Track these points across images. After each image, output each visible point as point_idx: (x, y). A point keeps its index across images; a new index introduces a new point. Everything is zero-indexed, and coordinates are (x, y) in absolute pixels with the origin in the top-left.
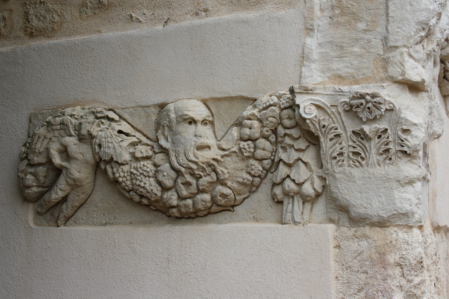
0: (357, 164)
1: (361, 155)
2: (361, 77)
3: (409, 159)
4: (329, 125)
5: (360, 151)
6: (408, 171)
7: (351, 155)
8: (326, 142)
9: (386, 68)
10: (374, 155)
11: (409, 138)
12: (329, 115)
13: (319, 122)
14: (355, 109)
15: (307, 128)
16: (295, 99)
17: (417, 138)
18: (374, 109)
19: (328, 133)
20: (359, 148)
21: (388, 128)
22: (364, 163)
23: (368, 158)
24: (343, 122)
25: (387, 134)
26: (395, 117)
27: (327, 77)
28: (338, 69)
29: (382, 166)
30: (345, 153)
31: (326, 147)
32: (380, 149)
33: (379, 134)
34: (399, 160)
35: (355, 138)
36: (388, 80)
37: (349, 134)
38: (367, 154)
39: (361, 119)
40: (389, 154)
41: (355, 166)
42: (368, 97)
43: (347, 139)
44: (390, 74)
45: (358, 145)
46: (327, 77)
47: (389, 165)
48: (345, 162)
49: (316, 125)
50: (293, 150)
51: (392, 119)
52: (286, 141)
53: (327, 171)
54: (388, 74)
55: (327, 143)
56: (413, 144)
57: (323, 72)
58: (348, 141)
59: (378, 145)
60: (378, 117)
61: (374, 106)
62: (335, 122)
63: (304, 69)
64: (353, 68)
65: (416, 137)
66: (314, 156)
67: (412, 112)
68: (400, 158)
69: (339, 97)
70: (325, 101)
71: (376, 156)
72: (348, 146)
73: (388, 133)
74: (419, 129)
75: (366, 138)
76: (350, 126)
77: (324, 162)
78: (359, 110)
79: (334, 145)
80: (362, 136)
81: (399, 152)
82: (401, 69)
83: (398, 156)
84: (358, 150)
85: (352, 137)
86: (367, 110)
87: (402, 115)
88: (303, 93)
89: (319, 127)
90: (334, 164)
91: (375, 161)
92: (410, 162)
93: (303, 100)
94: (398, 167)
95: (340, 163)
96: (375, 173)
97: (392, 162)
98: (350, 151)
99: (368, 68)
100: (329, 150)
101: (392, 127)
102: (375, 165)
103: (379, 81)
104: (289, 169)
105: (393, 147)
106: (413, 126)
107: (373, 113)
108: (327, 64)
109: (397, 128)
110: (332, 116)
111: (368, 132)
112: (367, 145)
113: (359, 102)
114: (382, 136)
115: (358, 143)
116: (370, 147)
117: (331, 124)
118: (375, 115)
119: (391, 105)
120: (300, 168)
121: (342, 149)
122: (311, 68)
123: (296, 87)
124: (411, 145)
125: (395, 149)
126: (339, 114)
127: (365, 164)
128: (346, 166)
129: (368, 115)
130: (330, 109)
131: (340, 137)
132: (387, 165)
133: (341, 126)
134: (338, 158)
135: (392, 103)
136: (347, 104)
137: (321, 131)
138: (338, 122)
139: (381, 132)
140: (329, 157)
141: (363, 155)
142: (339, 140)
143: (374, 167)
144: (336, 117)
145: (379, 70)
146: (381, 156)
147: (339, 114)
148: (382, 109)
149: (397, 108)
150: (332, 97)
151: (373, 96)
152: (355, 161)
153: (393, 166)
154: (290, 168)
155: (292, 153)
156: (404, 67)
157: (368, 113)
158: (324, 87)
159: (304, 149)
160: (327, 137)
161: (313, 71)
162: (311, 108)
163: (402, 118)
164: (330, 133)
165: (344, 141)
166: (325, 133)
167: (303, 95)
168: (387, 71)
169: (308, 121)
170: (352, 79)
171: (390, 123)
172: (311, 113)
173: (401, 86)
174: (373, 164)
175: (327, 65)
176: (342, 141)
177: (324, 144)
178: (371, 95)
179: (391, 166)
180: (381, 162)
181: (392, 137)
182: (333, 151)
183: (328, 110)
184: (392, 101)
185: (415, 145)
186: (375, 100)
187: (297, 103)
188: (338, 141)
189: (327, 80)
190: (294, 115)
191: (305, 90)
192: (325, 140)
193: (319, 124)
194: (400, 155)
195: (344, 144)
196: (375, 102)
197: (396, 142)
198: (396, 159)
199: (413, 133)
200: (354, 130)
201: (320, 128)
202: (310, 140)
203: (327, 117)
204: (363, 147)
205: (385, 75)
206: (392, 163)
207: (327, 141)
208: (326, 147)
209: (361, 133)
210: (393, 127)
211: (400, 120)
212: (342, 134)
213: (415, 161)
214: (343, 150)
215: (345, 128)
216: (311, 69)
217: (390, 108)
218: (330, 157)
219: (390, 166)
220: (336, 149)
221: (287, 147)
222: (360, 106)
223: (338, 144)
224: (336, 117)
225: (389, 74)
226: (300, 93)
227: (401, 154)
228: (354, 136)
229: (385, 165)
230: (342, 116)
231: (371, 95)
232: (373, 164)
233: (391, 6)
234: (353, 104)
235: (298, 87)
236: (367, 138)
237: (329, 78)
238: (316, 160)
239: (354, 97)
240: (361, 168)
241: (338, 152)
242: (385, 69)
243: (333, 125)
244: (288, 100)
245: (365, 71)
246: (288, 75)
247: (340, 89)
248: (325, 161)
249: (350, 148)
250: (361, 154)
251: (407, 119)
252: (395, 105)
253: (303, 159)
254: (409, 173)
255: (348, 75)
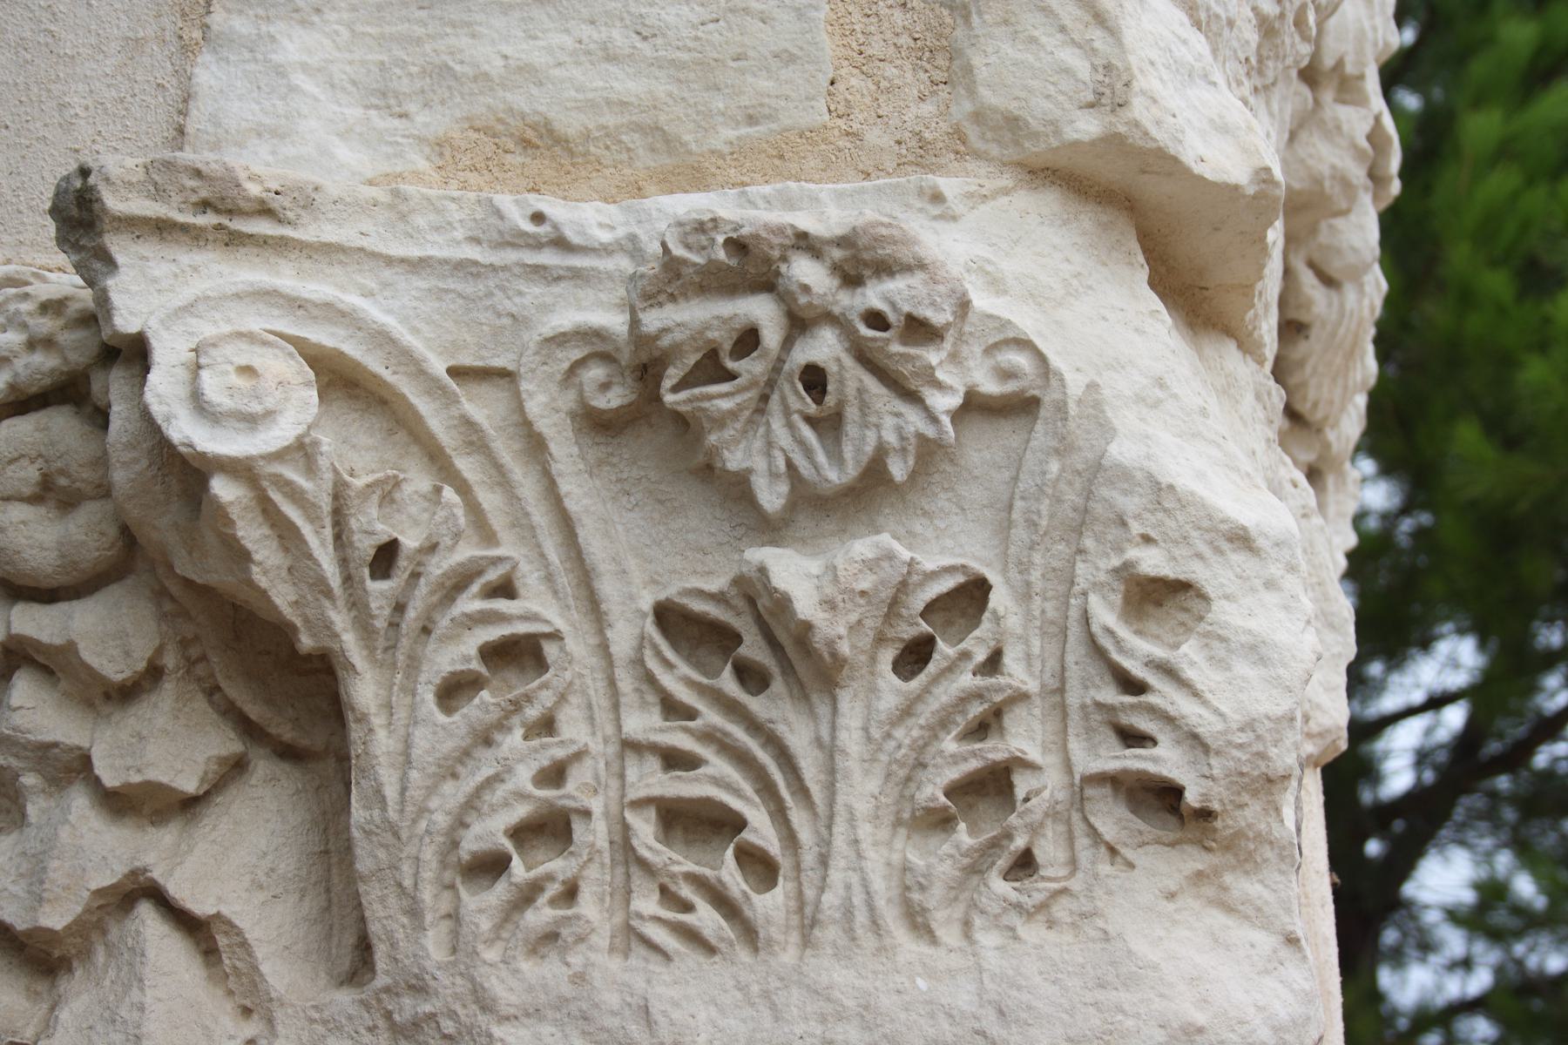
0: (706, 917)
1: (746, 835)
2: (729, 133)
3: (1194, 860)
4: (432, 548)
5: (737, 792)
6: (1193, 981)
7: (645, 829)
8: (401, 714)
9: (953, 54)
10: (865, 831)
11: (1190, 655)
12: (436, 458)
13: (339, 516)
14: (683, 395)
15: (215, 574)
16: (110, 283)
17: (1263, 661)
18: (861, 391)
19: (426, 631)
20: (719, 765)
21: (993, 577)
22: (769, 905)
23: (809, 858)
24: (566, 524)
25: (985, 628)
26: (1054, 467)
27: (421, 140)
28: (527, 71)
29: (949, 935)
30: (586, 814)
31: (406, 759)
32: (922, 775)
33: (908, 632)
34: (1105, 868)
35: (678, 678)
36: (978, 155)
37: (622, 639)
38: (798, 817)
39: (738, 490)
40: (1013, 819)
41: (692, 936)
42: (806, 272)
43: (612, 683)
44: (987, 96)
45: (710, 736)
46: (421, 140)
47: (1013, 919)
48: (588, 906)
49: (307, 530)
50: (79, 802)
51: (1026, 483)
52: (18, 719)
53: (407, 1001)
54: (972, 92)
55: (414, 721)
56: (1236, 718)
57: (384, 98)
58: (616, 707)
59: (899, 733)
60: (898, 470)
61: (865, 357)
62: (497, 521)
63: (208, 74)
64: (658, 63)
65: (1257, 651)
66: (287, 865)
67: (1196, 435)
68: (1113, 851)
69: (535, 291)
70: (404, 320)
71: (889, 844)
72: (612, 749)
73: (997, 619)
74: (1270, 585)
75: (788, 669)
76: (632, 563)
77: (383, 914)
78: (720, 398)
79: (485, 739)
80: (753, 648)
81: (1107, 790)
82: (1087, 49)
83: (1094, 833)
84: (717, 781)
85: (652, 664)
86: (794, 404)
87: (1122, 451)
88: (184, 228)
89: (344, 562)
90: (485, 924)
91: (878, 884)
92: (1209, 891)
93: (187, 294)
94: (1106, 937)
95: (540, 915)
96: (886, 1001)
97: (1037, 890)
98: (633, 794)
99: (792, 59)
100: (431, 790)
101: (1024, 567)
102: (875, 925)
103: (890, 165)
104: (34, 996)
105: (1045, 750)
106: (1218, 551)
107: (851, 429)
108: (419, 31)
109: (1081, 568)
110: (467, 466)
111: (806, 605)
112: (799, 738)
113: (724, 321)
114: (941, 644)
115: (711, 717)
116: (829, 751)
117: (457, 536)
118: (869, 449)
119: (1021, 360)
120: (147, 972)
121: (555, 775)
122: (277, 58)
123: (114, 171)
124: (1220, 727)
125: (1068, 766)
126: (535, 446)
127: (779, 916)
128: (601, 940)
129: (808, 453)
130: (450, 399)
131: (541, 665)
132: (996, 922)
133: (554, 556)
134: (519, 870)
135: (1024, 344)
136: (606, 358)
137: (358, 606)
138: (522, 524)
139: (929, 610)
140: (429, 854)
141: (761, 830)
142: (528, 698)
143: (868, 941)
144: (502, 479)
145: (890, 71)
146: (934, 840)
147: (535, 446)
148: (939, 385)
149: (1075, 385)
150: (468, 288)
151: (857, 260)
152: (686, 891)
153: (1051, 936)
154: (41, 986)
155: (64, 834)
156: (1113, 32)
157: (807, 432)
158: (396, 193)
159: (189, 784)
160: (414, 664)
161: (293, 89)
162: (256, 363)
163: (1123, 475)
164: (443, 623)
165: (574, 700)
166: (394, 625)
167: (188, 257)
168: (969, 70)
169: (223, 489)
170: (645, 159)
171: (1010, 524)
172: (256, 408)
173: (1088, 218)
174: (861, 918)
175: (419, 41)
176: (562, 698)
177: (381, 734)
178: (837, 254)
179: (1032, 933)
180: (938, 891)
181: (1028, 657)
182: (472, 804)
183: (424, 406)
184: (1026, 321)
185: (1249, 725)
186: (874, 295)
187: (126, 321)
188: (517, 706)
189: (422, 165)
190: (102, 461)
191: (205, 205)
192: (401, 701)
193: (338, 537)
194: (1111, 818)
195: (573, 729)
196: (876, 320)
197: (1073, 699)
198: (1073, 863)
199: (1227, 614)
200: (670, 592)
201: (348, 579)
202: (254, 711)
203: (418, 481)
204: (764, 757)
205: (944, 112)
206: (1043, 907)
207: (413, 708)
208: (406, 759)
209: (743, 624)
210: (1037, 558)
211: (1105, 492)
212: (555, 636)
213: (1244, 886)
214: (574, 790)
215: (585, 576)
216: (280, 71)
217: (1010, 387)
218: (444, 865)
219: (1022, 931)
220: (496, 779)
221: (29, 780)
222: (730, 365)
223: (518, 733)
224: (502, 479)
225: (985, 93)
226: (162, 228)
227: (1122, 811)
228: (669, 654)
229: (978, 921)
230: (555, 468)
231: (837, 254)
232: (861, 918)
233: (609, 402)
234: (665, 342)
235: (140, 175)
236: (802, 669)
237: (440, 146)
238: (311, 905)
239: (672, 266)
240: (743, 955)
241: (521, 812)
242: (941, 61)
243: (466, 552)
244: (45, 325)
245: (765, 84)
246: (67, 126)
247: (538, 218)
248: (392, 900)
249: (632, 773)
250: (737, 824)
251: (1165, 480)
252: (1055, 361)
253: (179, 889)
254: (1204, 1001)
255: (610, 120)
